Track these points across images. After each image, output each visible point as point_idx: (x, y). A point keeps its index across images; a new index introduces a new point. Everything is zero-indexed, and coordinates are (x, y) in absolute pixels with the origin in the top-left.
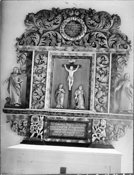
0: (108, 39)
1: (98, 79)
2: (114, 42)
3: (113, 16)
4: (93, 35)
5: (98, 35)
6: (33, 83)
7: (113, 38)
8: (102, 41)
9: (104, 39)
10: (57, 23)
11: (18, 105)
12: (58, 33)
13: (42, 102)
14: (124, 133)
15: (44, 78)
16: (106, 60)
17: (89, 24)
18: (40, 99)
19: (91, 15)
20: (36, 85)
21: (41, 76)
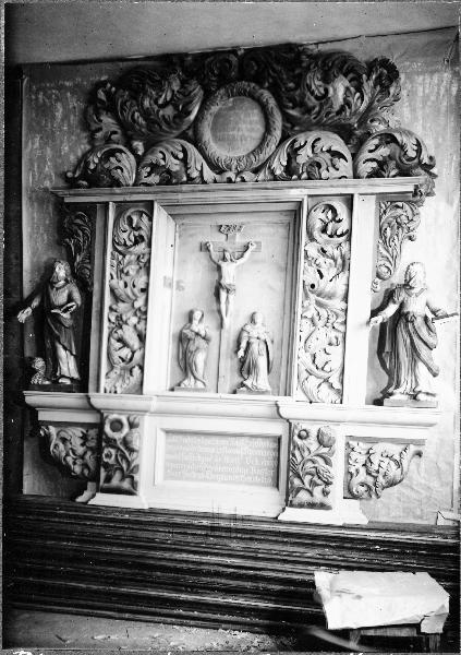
0: (354, 156)
1: (313, 286)
2: (375, 165)
3: (372, 66)
4: (301, 147)
5: (319, 145)
6: (111, 309)
7: (371, 151)
8: (334, 166)
9: (341, 156)
10: (181, 155)
11: (68, 382)
12: (189, 146)
13: (136, 371)
14: (343, 278)
15: (142, 290)
16: (340, 221)
17: (297, 145)
18: (131, 359)
19: (297, 72)
20: (119, 318)
21: (134, 286)
